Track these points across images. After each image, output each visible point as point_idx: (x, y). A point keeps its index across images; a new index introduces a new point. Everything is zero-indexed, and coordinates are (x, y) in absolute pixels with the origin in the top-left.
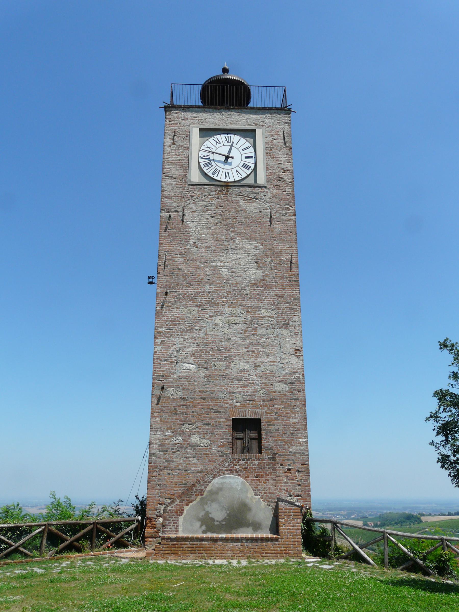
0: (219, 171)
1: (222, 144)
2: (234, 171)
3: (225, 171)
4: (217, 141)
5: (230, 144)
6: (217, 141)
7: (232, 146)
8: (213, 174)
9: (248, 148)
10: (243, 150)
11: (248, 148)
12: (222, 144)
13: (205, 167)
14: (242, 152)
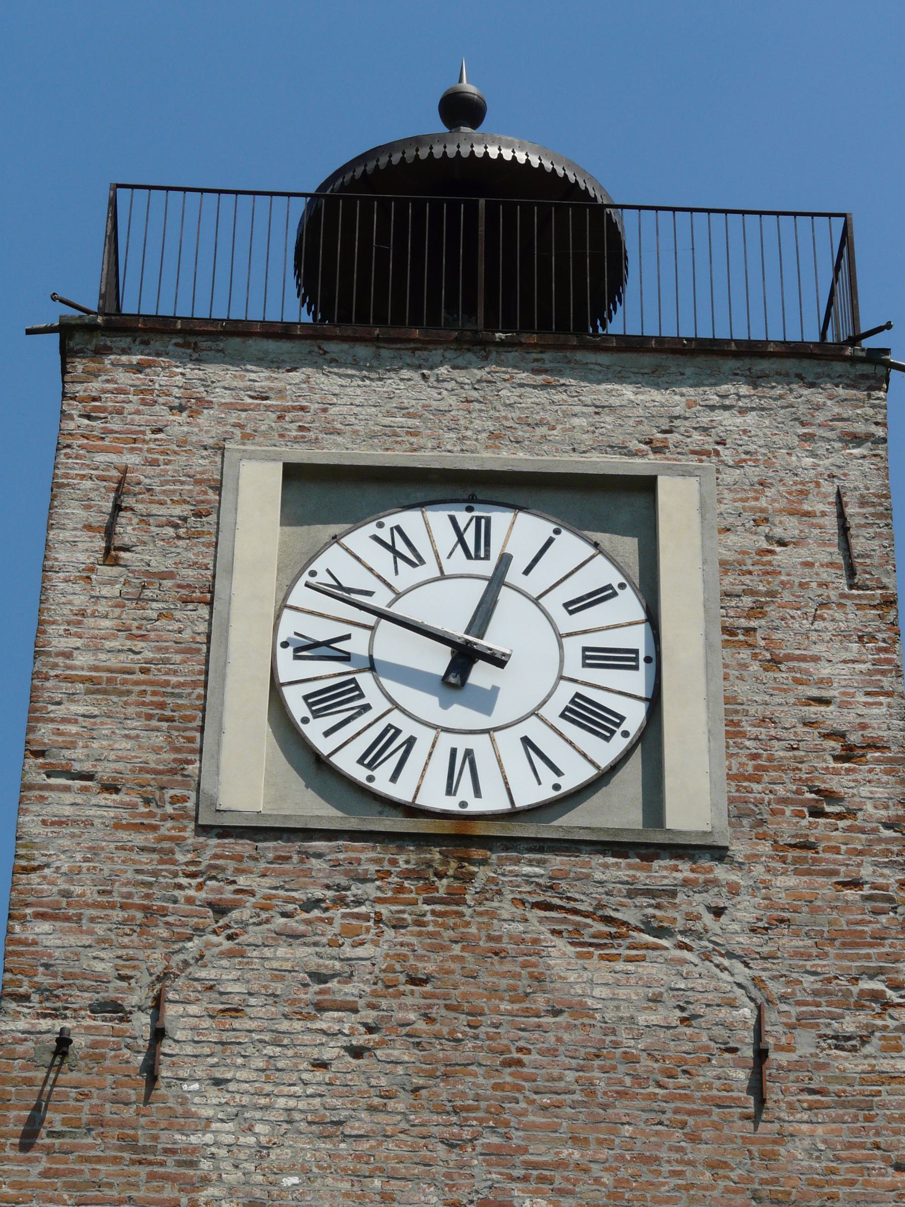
1: (429, 570)
2: (509, 742)
3: (447, 741)
4: (401, 546)
5: (487, 568)
6: (401, 546)
7: (497, 581)
8: (370, 760)
9: (603, 595)
10: (574, 606)
11: (603, 595)
12: (429, 570)
13: (316, 714)
14: (567, 622)
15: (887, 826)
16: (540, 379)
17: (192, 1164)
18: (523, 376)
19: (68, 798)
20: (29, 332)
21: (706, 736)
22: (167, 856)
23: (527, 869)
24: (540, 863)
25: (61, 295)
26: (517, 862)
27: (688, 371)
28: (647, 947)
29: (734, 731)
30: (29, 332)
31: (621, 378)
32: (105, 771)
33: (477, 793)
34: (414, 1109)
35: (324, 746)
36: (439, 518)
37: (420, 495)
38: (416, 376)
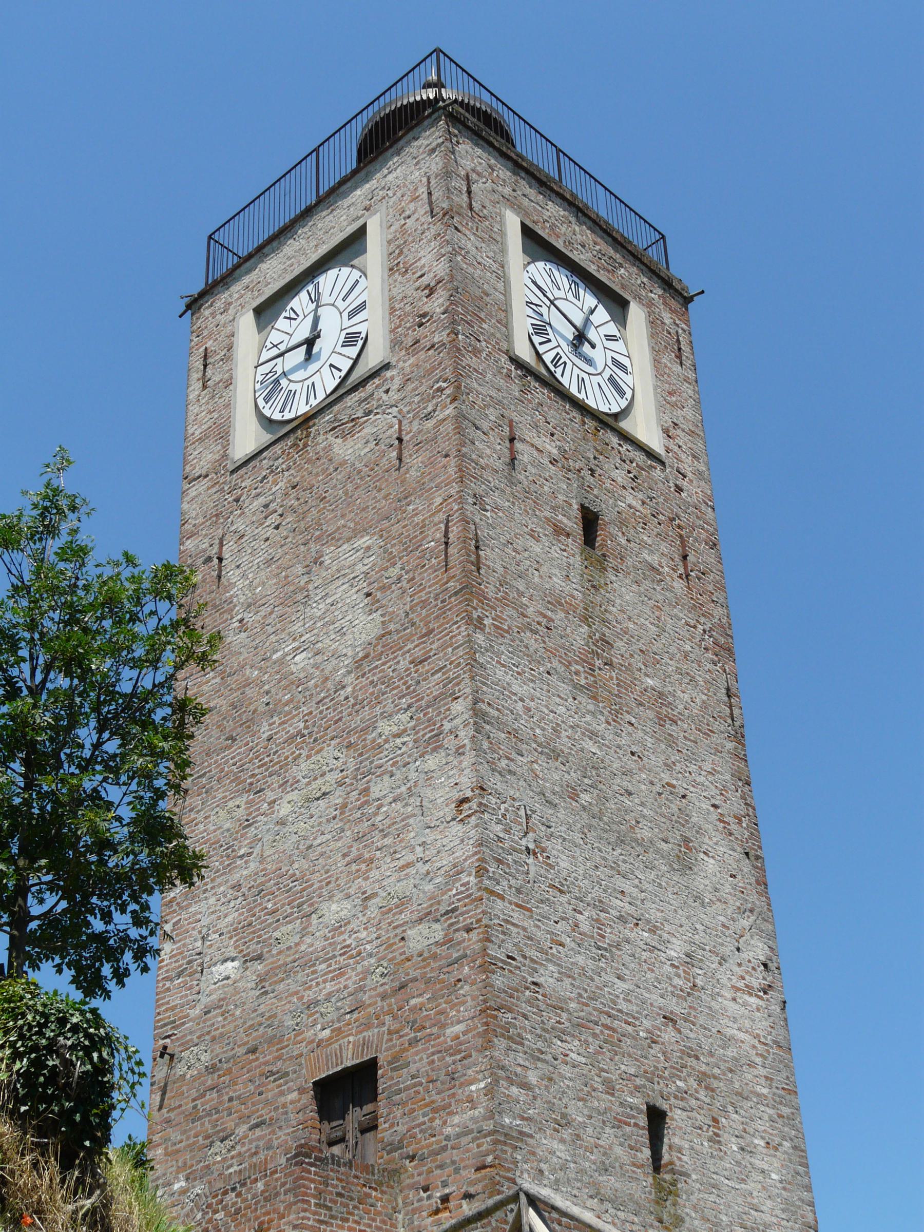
0: (549, 341)
15: (443, 314)
16: (329, 210)
17: (231, 602)
18: (324, 213)
19: (194, 489)
20: (180, 316)
21: (813, 1186)
22: (222, 490)
23: (327, 418)
24: (331, 413)
25: (184, 295)
26: (324, 417)
27: (377, 167)
28: (365, 422)
29: (392, 310)
30: (180, 316)
31: (356, 188)
32: (204, 472)
33: (340, 370)
34: (294, 538)
35: (541, 349)
36: (565, 381)
37: (293, 293)
38: (291, 241)
